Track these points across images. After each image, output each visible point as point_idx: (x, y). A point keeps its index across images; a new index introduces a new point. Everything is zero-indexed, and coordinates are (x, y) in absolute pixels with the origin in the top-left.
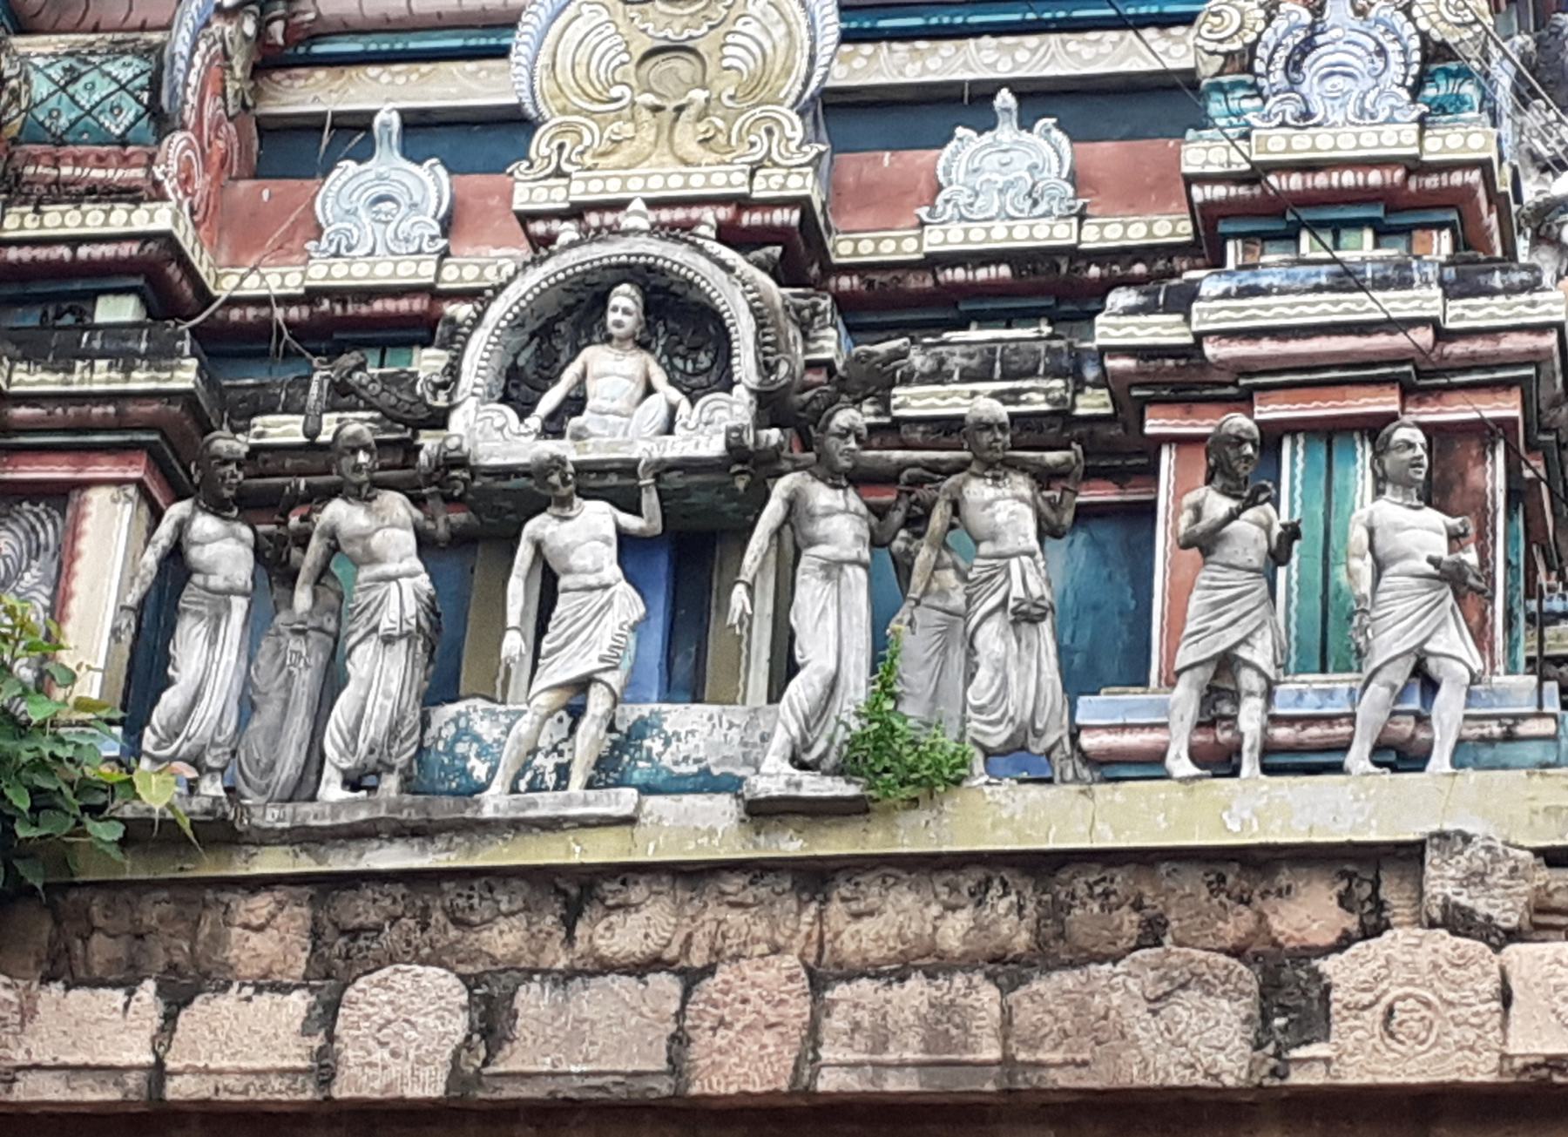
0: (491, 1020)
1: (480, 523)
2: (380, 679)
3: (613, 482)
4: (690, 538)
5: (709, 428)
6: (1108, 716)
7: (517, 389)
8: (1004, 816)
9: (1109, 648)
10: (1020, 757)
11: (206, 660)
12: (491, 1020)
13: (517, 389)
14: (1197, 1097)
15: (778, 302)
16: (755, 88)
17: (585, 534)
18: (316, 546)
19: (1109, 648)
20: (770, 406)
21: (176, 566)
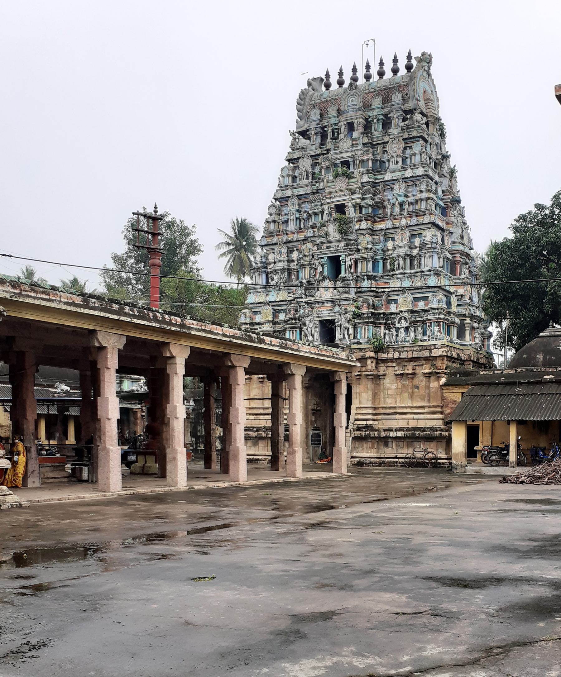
0: (400, 355)
1: (397, 330)
2: (394, 338)
3: (403, 328)
4: (407, 329)
5: (407, 325)
6: (424, 338)
7: (399, 323)
8: (420, 343)
9: (425, 333)
10: (421, 341)
11: (387, 337)
12: (400, 355)
13: (399, 323)
14: (204, 351)
15: (458, 366)
16: (409, 303)
17: (402, 330)
18: (184, 247)
19: (425, 333)
20: (409, 324)
21: (385, 333)
